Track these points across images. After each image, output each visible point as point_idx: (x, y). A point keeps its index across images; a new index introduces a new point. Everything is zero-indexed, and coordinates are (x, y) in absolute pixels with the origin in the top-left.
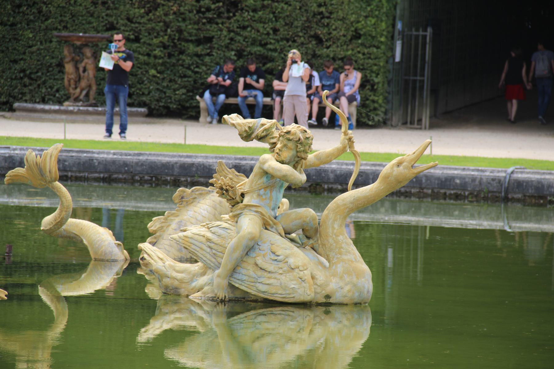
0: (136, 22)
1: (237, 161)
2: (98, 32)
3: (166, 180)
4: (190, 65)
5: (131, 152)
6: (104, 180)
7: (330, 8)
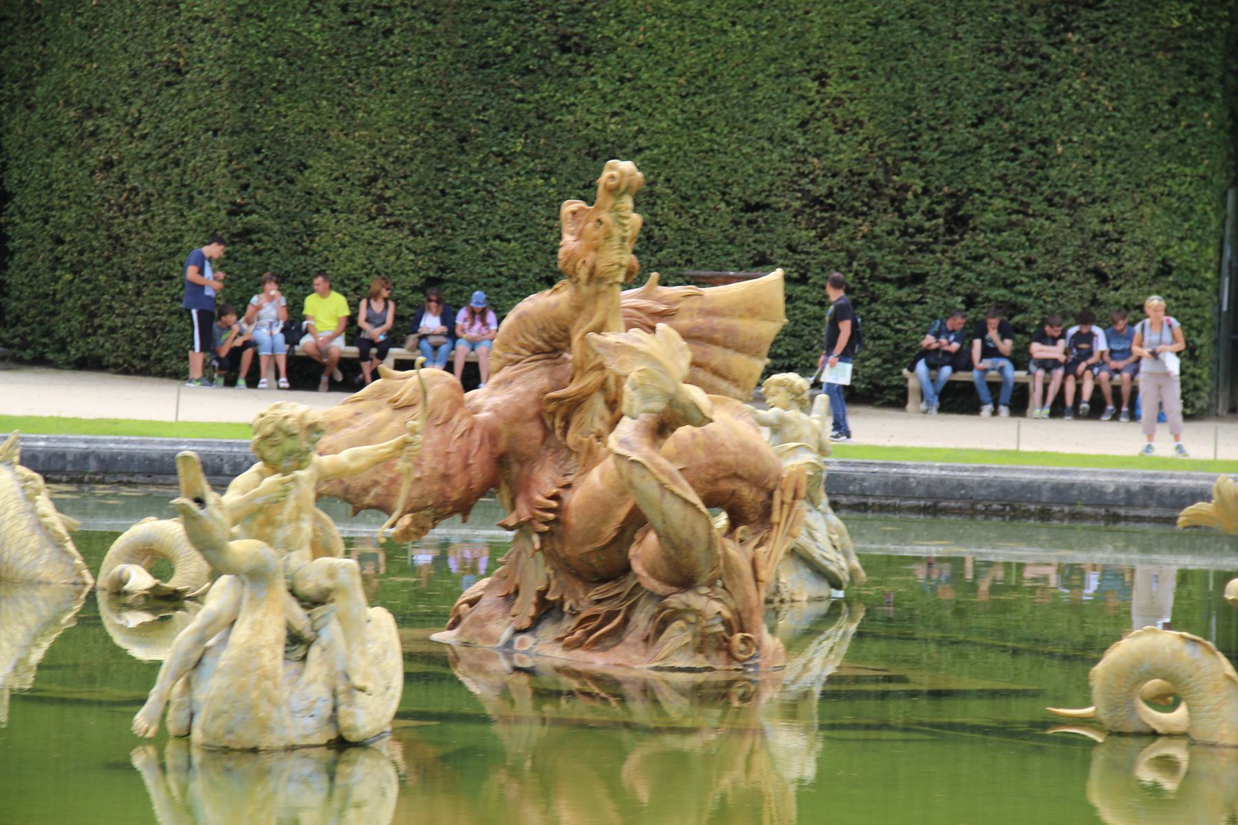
0: (802, 252)
1: (1147, 480)
2: (741, 269)
3: (1028, 511)
4: (887, 319)
5: (968, 465)
6: (924, 510)
7: (1121, 225)
